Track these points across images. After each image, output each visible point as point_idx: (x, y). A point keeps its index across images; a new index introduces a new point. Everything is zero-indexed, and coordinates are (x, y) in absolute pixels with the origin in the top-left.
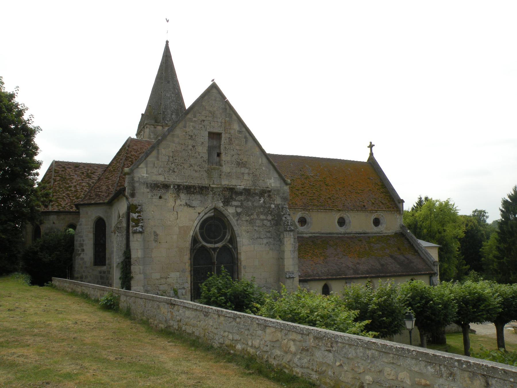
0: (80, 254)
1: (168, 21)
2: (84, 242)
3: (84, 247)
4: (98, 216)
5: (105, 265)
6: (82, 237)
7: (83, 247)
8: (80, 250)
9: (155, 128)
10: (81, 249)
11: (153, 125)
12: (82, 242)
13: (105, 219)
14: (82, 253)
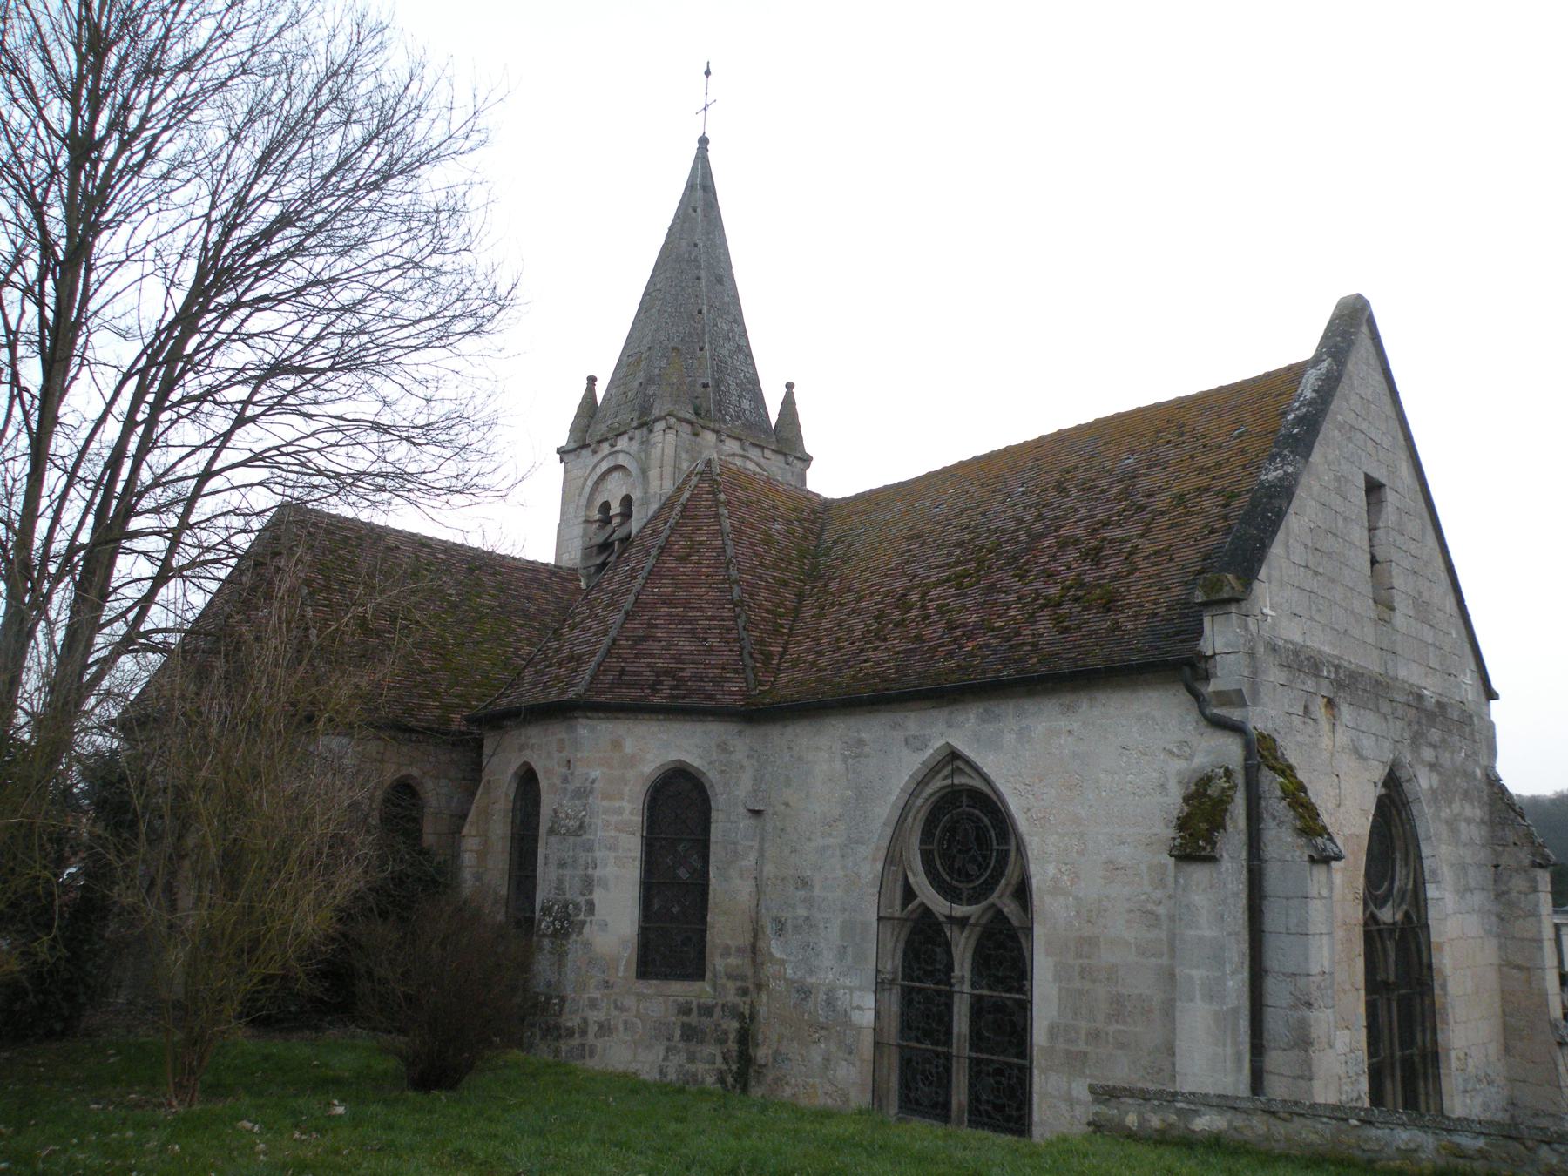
0: (583, 923)
1: (708, 73)
3: (598, 895)
4: (680, 761)
5: (702, 977)
6: (590, 849)
7: (591, 892)
9: (696, 434)
11: (691, 423)
12: (590, 871)
13: (712, 776)
14: (588, 919)
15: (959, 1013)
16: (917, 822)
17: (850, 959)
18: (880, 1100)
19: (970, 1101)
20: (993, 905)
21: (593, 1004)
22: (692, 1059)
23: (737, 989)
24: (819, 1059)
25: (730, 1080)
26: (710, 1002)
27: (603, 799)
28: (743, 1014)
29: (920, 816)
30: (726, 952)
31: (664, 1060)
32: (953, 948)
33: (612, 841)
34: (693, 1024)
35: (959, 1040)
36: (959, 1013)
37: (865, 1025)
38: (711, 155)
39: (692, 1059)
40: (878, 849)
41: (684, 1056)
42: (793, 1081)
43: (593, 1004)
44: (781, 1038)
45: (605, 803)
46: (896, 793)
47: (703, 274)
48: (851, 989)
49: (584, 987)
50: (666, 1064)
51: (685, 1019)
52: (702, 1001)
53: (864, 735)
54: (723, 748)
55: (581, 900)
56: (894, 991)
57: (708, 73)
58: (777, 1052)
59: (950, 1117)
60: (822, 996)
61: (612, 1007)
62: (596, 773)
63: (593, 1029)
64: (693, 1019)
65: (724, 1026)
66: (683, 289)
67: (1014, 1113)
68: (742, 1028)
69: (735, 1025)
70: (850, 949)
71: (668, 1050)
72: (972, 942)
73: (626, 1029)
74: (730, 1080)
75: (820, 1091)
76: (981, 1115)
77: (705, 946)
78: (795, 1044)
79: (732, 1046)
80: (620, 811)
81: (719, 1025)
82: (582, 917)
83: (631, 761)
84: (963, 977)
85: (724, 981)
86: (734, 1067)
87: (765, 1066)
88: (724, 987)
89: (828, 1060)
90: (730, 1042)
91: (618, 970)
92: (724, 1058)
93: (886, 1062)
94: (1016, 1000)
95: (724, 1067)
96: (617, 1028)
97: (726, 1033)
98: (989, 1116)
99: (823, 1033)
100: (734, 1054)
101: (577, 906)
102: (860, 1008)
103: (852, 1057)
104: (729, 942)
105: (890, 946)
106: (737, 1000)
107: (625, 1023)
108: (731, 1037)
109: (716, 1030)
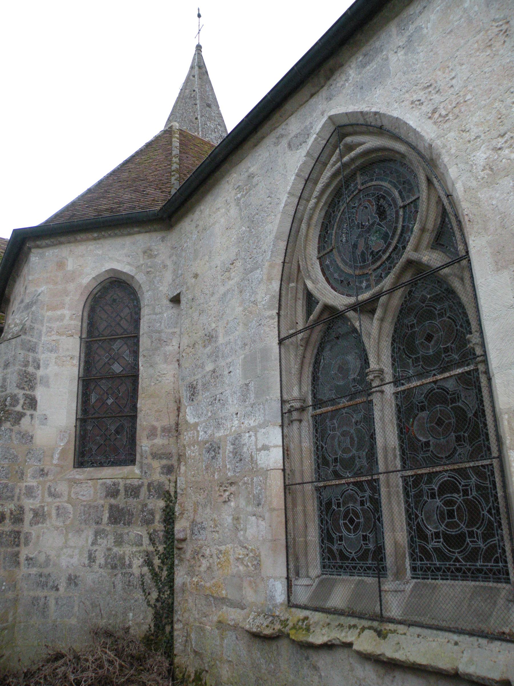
0: (21, 416)
1: (199, 16)
2: (40, 373)
3: (40, 393)
5: (133, 462)
6: (32, 349)
7: (32, 388)
8: (21, 402)
10: (26, 396)
12: (31, 369)
13: (140, 278)
14: (28, 413)
15: (382, 419)
16: (311, 231)
17: (252, 396)
18: (297, 559)
19: (412, 540)
20: (410, 263)
21: (30, 492)
22: (119, 541)
23: (163, 467)
24: (229, 520)
25: (157, 562)
26: (136, 482)
27: (48, 310)
28: (168, 492)
29: (314, 221)
30: (153, 433)
31: (93, 544)
32: (365, 339)
33: (54, 343)
34: (121, 506)
35: (386, 457)
36: (382, 419)
37: (272, 466)
38: (204, 54)
39: (119, 541)
40: (272, 266)
41: (111, 539)
42: (207, 552)
43: (30, 492)
44: (197, 504)
45: (50, 313)
46: (284, 198)
47: (198, 102)
48: (255, 430)
49: (22, 475)
50: (95, 548)
51: (113, 501)
52: (128, 482)
53: (252, 170)
54: (148, 253)
55: (20, 393)
56: (304, 423)
57: (199, 16)
58: (193, 523)
59: (384, 568)
60: (230, 448)
61: (46, 495)
62: (43, 288)
63: (28, 516)
64: (120, 501)
65: (150, 506)
66: (186, 110)
67: (481, 544)
68: (167, 507)
69: (161, 504)
70: (252, 385)
71: (97, 533)
72: (388, 328)
73: (58, 515)
74: (157, 562)
75: (232, 558)
76: (429, 558)
77: (135, 432)
78: (208, 510)
79: (159, 526)
80: (61, 318)
81: (146, 505)
82: (19, 408)
83: (71, 277)
84: (381, 371)
85: (150, 460)
86: (161, 548)
87: (184, 540)
88: (149, 466)
89: (238, 519)
90: (156, 523)
91: (52, 457)
92: (151, 539)
93: (299, 508)
94: (460, 377)
95: (151, 548)
96: (50, 514)
97: (152, 513)
98: (442, 556)
99: (233, 489)
100: (161, 534)
101: (15, 400)
102: (265, 448)
103: (260, 509)
104: (156, 424)
105: (295, 368)
106: (163, 479)
107: (58, 508)
108: (158, 517)
109: (143, 511)
